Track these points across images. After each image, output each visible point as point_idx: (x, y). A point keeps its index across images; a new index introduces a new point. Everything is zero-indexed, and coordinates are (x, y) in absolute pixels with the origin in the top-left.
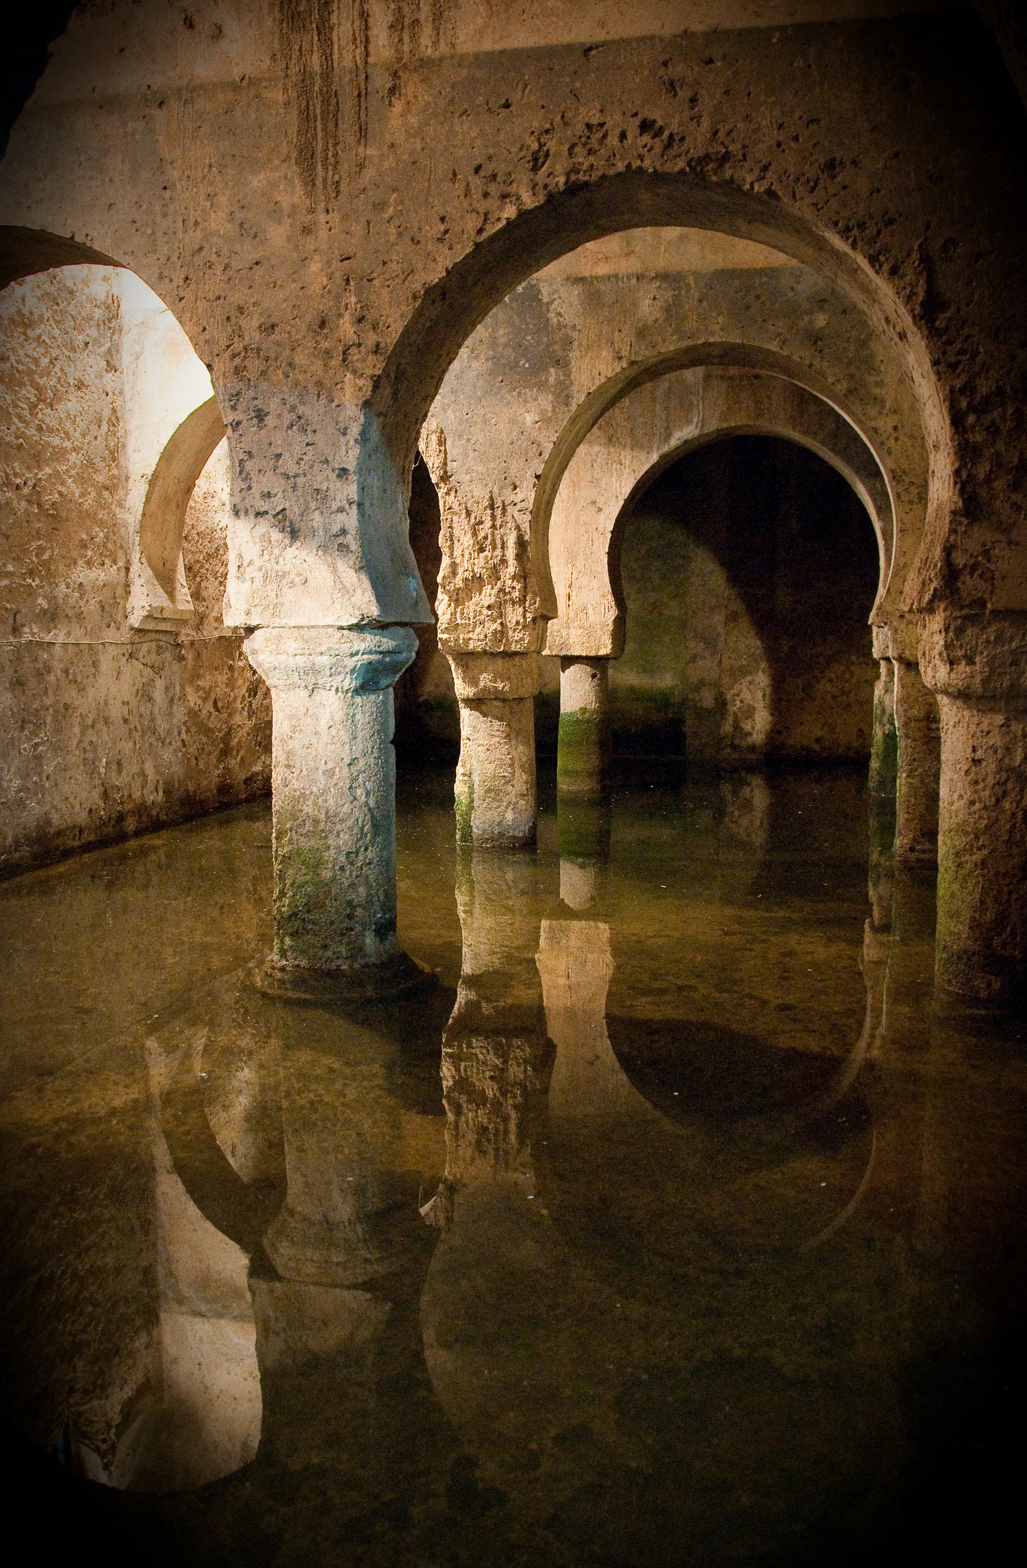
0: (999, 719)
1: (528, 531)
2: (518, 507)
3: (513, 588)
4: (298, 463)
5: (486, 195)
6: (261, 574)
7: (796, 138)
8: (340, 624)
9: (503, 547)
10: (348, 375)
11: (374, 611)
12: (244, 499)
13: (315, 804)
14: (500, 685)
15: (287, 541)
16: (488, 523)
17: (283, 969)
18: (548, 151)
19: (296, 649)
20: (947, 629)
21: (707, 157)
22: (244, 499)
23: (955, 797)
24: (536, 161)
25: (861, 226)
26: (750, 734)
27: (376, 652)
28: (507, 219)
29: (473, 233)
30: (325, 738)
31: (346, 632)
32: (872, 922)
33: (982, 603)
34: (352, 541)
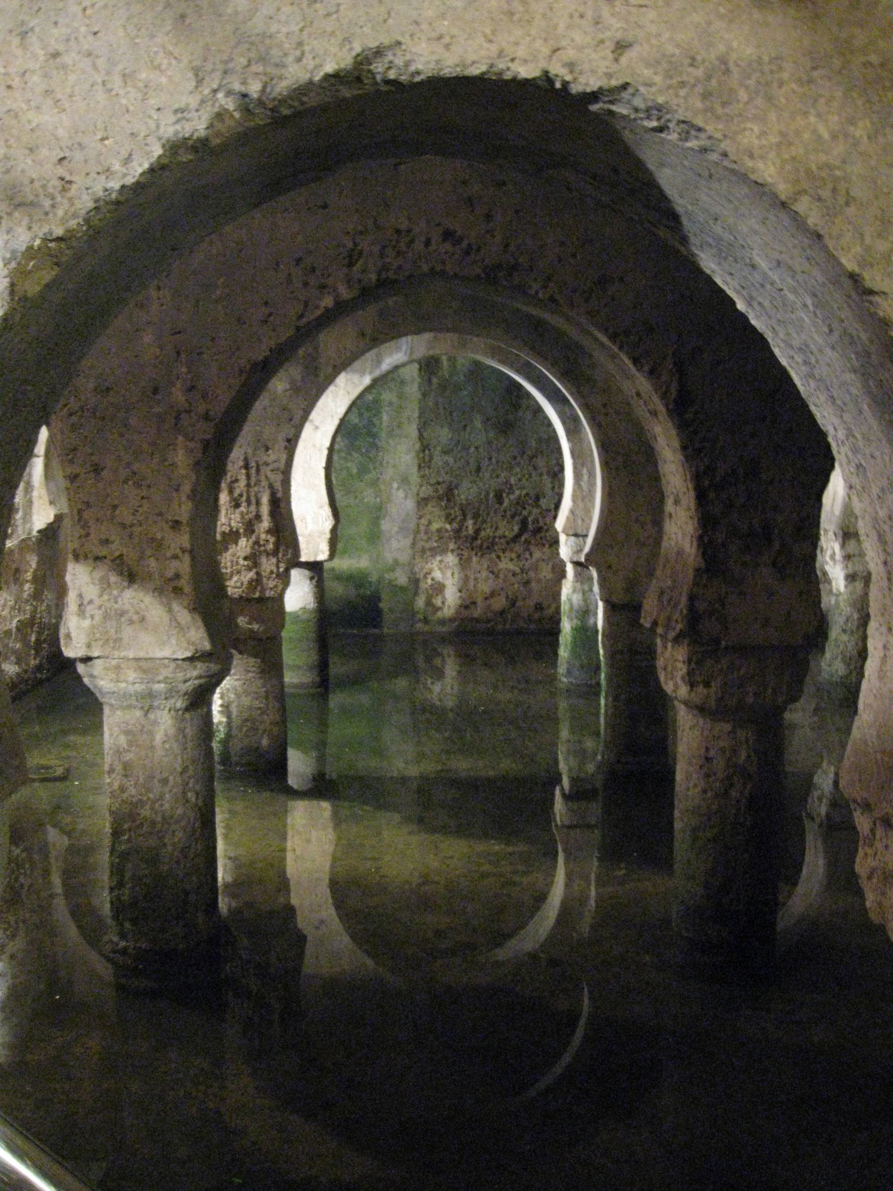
0: (727, 727)
1: (280, 489)
2: (271, 467)
3: (267, 541)
4: (133, 514)
5: (306, 284)
6: (101, 612)
7: (574, 256)
8: (175, 656)
9: (258, 503)
10: (180, 438)
11: (207, 646)
12: (82, 545)
13: (152, 809)
14: (255, 627)
15: (126, 584)
16: (243, 483)
17: (124, 952)
18: (362, 251)
19: (135, 678)
20: (690, 661)
21: (499, 266)
22: (82, 545)
23: (691, 785)
24: (351, 259)
25: (627, 333)
26: (440, 609)
27: (204, 677)
28: (325, 308)
29: (294, 318)
30: (160, 752)
31: (180, 662)
32: (562, 789)
33: (717, 642)
34: (185, 583)
